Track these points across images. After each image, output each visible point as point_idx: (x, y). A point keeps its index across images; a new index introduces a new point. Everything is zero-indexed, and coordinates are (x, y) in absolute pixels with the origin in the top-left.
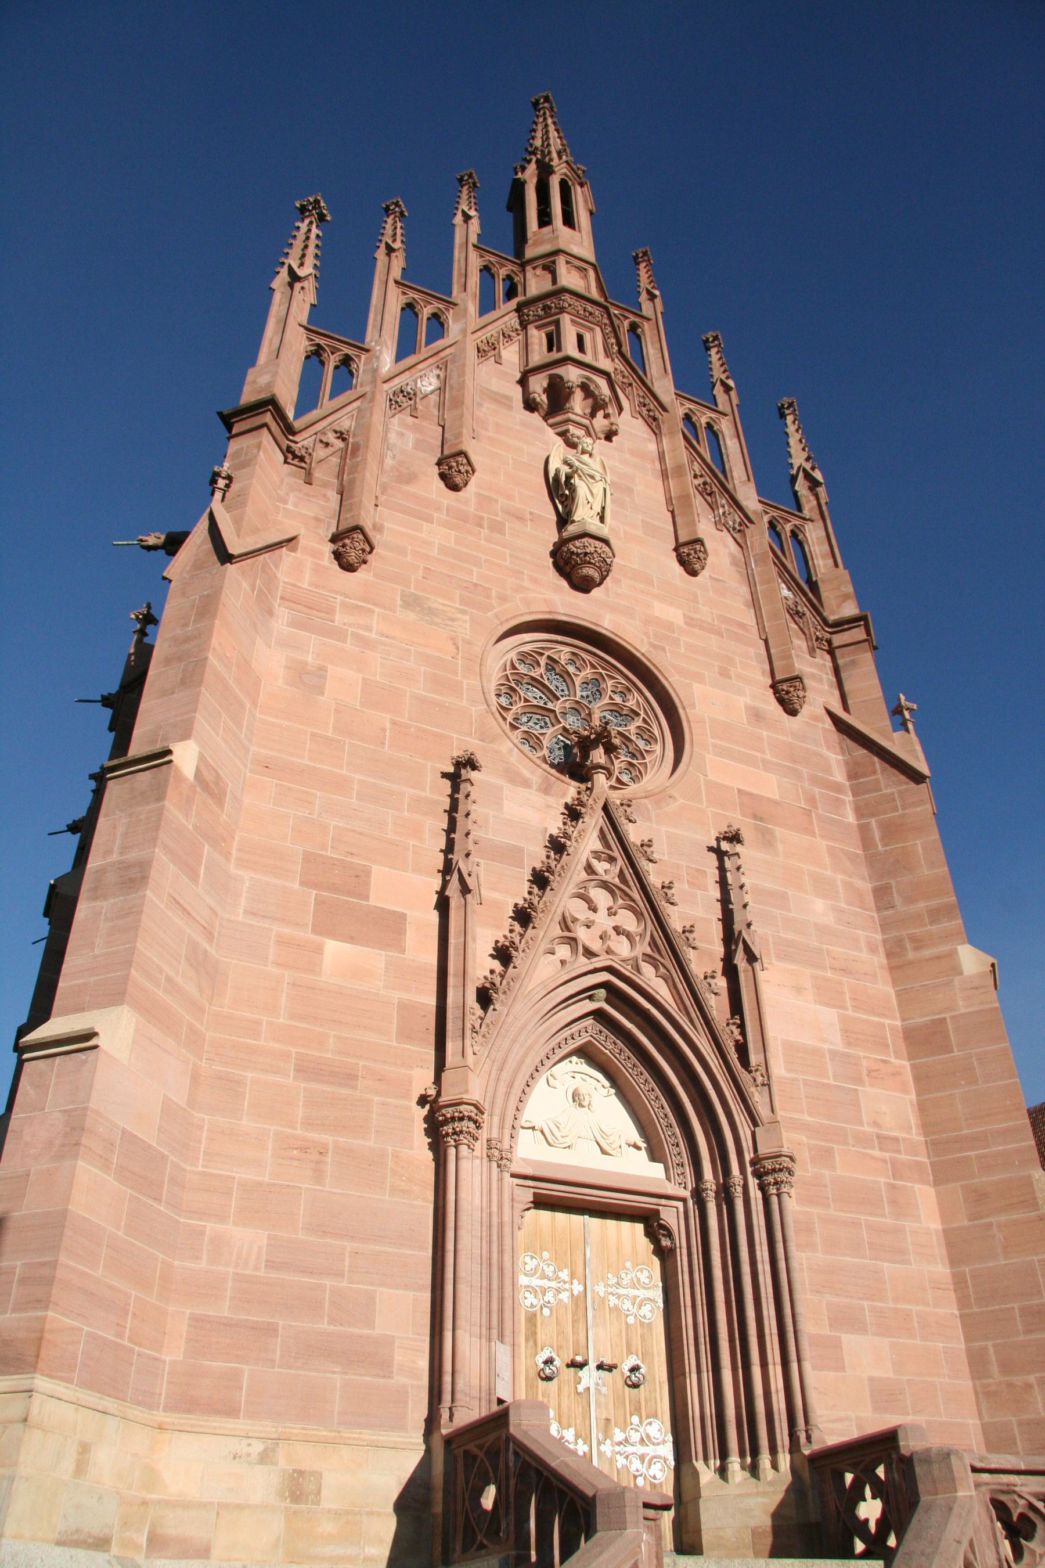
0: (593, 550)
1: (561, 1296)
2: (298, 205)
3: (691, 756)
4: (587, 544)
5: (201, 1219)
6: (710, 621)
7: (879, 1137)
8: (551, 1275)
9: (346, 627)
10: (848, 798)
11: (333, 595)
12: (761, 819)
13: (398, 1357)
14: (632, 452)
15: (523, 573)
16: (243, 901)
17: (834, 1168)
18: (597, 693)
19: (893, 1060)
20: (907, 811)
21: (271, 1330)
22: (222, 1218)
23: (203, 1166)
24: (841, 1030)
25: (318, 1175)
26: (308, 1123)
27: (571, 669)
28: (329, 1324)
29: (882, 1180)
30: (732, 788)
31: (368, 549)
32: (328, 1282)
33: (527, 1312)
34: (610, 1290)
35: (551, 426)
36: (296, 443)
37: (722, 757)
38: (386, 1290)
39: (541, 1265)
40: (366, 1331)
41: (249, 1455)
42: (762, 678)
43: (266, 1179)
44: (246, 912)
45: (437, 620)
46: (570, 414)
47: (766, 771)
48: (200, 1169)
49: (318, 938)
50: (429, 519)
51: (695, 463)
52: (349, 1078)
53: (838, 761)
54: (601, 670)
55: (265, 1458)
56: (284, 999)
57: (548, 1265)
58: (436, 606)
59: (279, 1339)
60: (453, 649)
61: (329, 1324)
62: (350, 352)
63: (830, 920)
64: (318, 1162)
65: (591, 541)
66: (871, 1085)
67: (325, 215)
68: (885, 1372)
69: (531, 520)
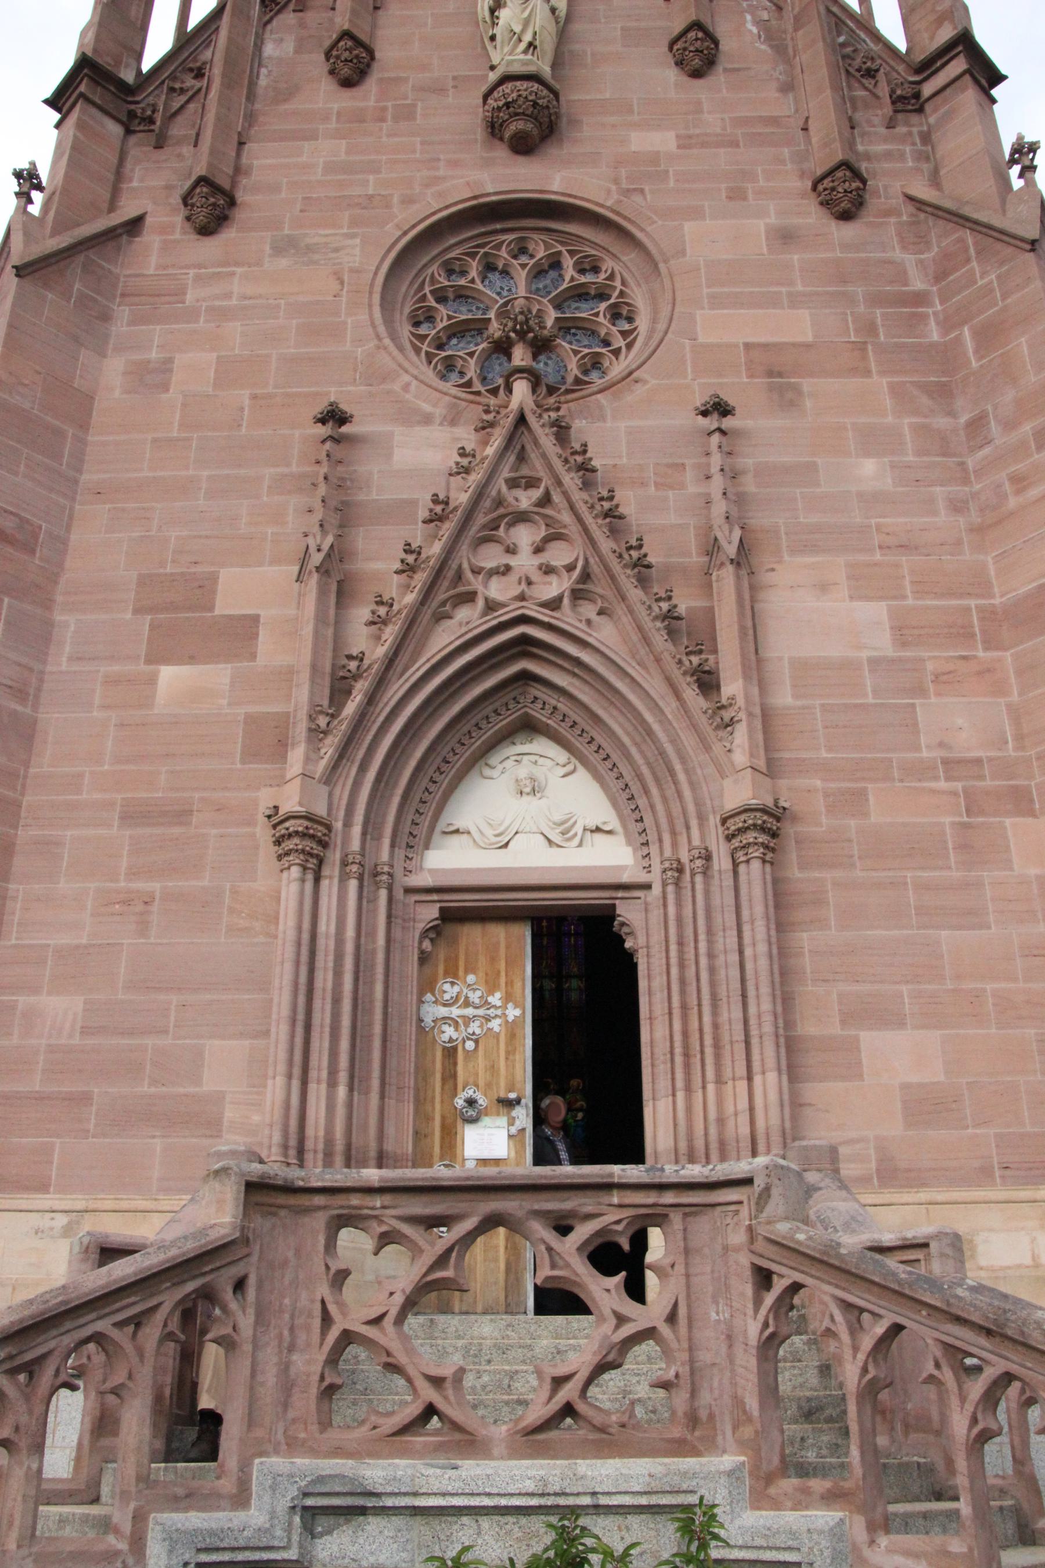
1: (490, 1025)
5: (13, 994)
6: (718, 130)
7: (946, 762)
8: (477, 1001)
11: (246, 302)
12: (780, 375)
13: (230, 1114)
15: (439, 160)
16: (67, 649)
17: (866, 815)
19: (981, 654)
20: (1009, 300)
21: (85, 1098)
22: (35, 990)
23: (17, 939)
24: (892, 628)
25: (143, 927)
26: (133, 873)
28: (150, 1085)
29: (948, 820)
30: (736, 346)
32: (149, 1041)
33: (444, 1048)
34: (499, 1012)
36: (137, 103)
38: (217, 1042)
39: (465, 991)
40: (192, 1090)
41: (52, 1229)
42: (799, 184)
43: (84, 941)
44: (70, 659)
45: (316, 257)
48: (14, 942)
49: (152, 667)
50: (313, 136)
52: (182, 815)
54: (482, 251)
55: (67, 1231)
56: (110, 743)
57: (474, 990)
58: (316, 240)
59: (94, 1108)
60: (335, 286)
61: (150, 1085)
63: (887, 483)
64: (142, 914)
66: (938, 694)
68: (935, 1073)
69: (455, 87)
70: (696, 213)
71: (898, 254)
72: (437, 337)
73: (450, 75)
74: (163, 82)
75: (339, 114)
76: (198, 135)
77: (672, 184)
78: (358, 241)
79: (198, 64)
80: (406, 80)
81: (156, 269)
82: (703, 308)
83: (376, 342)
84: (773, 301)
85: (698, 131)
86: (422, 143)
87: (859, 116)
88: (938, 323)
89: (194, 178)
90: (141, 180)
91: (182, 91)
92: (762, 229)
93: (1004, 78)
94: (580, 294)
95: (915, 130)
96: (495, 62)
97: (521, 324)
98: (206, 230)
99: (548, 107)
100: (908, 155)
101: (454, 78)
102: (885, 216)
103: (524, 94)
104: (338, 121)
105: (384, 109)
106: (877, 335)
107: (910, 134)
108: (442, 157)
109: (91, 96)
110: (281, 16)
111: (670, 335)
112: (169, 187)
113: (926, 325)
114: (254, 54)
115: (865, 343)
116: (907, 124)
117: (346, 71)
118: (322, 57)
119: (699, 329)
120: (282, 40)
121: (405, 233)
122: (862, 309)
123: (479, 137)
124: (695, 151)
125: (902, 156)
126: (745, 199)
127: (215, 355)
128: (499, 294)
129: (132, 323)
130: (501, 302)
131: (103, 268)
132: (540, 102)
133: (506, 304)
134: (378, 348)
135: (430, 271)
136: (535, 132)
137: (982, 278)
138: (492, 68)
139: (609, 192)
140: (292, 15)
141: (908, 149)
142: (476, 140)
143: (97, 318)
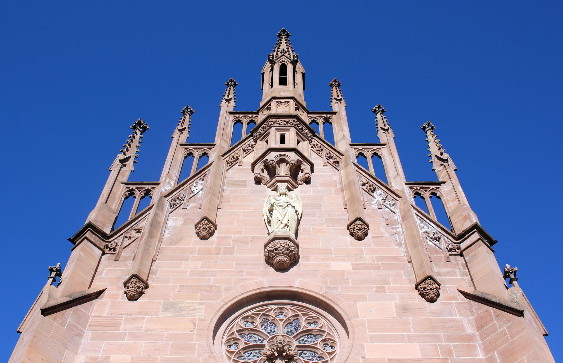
0: (279, 245)
2: (131, 127)
4: (275, 243)
6: (371, 262)
9: (126, 332)
10: (478, 343)
11: (121, 316)
14: (321, 185)
18: (272, 324)
20: (514, 339)
30: (384, 360)
35: (269, 188)
37: (377, 342)
42: (409, 285)
45: (184, 313)
46: (277, 178)
47: (411, 342)
51: (363, 177)
53: (469, 321)
54: (262, 313)
62: (147, 188)
67: (146, 127)
69: (251, 241)
72: (239, 353)
74: (122, 234)
75: (199, 250)
76: (134, 256)
77: (350, 285)
78: (204, 306)
79: (139, 228)
80: (230, 237)
81: (107, 314)
82: (368, 342)
83: (209, 354)
85: (362, 262)
86: (236, 264)
88: (481, 350)
89: (130, 275)
91: (130, 238)
92: (394, 305)
94: (307, 332)
96: (270, 232)
97: (280, 348)
98: (132, 299)
100: (458, 273)
101: (252, 237)
102: (450, 300)
103: (283, 245)
104: (198, 254)
105: (220, 249)
106: (453, 356)
108: (245, 270)
109: (90, 238)
111: (352, 355)
112: (118, 278)
114: (163, 225)
118: (194, 227)
119: (366, 352)
120: (176, 219)
121: (226, 303)
122: (444, 343)
126: (385, 292)
127: (130, 356)
128: (269, 333)
129: (94, 338)
130: (270, 337)
131: (82, 312)
132: (290, 248)
133: (272, 338)
134: (210, 357)
135: (237, 321)
136: (288, 261)
137: (500, 328)
138: (269, 234)
139: (321, 287)
140: (182, 210)
141: (457, 271)
142: (261, 264)
143: (76, 335)
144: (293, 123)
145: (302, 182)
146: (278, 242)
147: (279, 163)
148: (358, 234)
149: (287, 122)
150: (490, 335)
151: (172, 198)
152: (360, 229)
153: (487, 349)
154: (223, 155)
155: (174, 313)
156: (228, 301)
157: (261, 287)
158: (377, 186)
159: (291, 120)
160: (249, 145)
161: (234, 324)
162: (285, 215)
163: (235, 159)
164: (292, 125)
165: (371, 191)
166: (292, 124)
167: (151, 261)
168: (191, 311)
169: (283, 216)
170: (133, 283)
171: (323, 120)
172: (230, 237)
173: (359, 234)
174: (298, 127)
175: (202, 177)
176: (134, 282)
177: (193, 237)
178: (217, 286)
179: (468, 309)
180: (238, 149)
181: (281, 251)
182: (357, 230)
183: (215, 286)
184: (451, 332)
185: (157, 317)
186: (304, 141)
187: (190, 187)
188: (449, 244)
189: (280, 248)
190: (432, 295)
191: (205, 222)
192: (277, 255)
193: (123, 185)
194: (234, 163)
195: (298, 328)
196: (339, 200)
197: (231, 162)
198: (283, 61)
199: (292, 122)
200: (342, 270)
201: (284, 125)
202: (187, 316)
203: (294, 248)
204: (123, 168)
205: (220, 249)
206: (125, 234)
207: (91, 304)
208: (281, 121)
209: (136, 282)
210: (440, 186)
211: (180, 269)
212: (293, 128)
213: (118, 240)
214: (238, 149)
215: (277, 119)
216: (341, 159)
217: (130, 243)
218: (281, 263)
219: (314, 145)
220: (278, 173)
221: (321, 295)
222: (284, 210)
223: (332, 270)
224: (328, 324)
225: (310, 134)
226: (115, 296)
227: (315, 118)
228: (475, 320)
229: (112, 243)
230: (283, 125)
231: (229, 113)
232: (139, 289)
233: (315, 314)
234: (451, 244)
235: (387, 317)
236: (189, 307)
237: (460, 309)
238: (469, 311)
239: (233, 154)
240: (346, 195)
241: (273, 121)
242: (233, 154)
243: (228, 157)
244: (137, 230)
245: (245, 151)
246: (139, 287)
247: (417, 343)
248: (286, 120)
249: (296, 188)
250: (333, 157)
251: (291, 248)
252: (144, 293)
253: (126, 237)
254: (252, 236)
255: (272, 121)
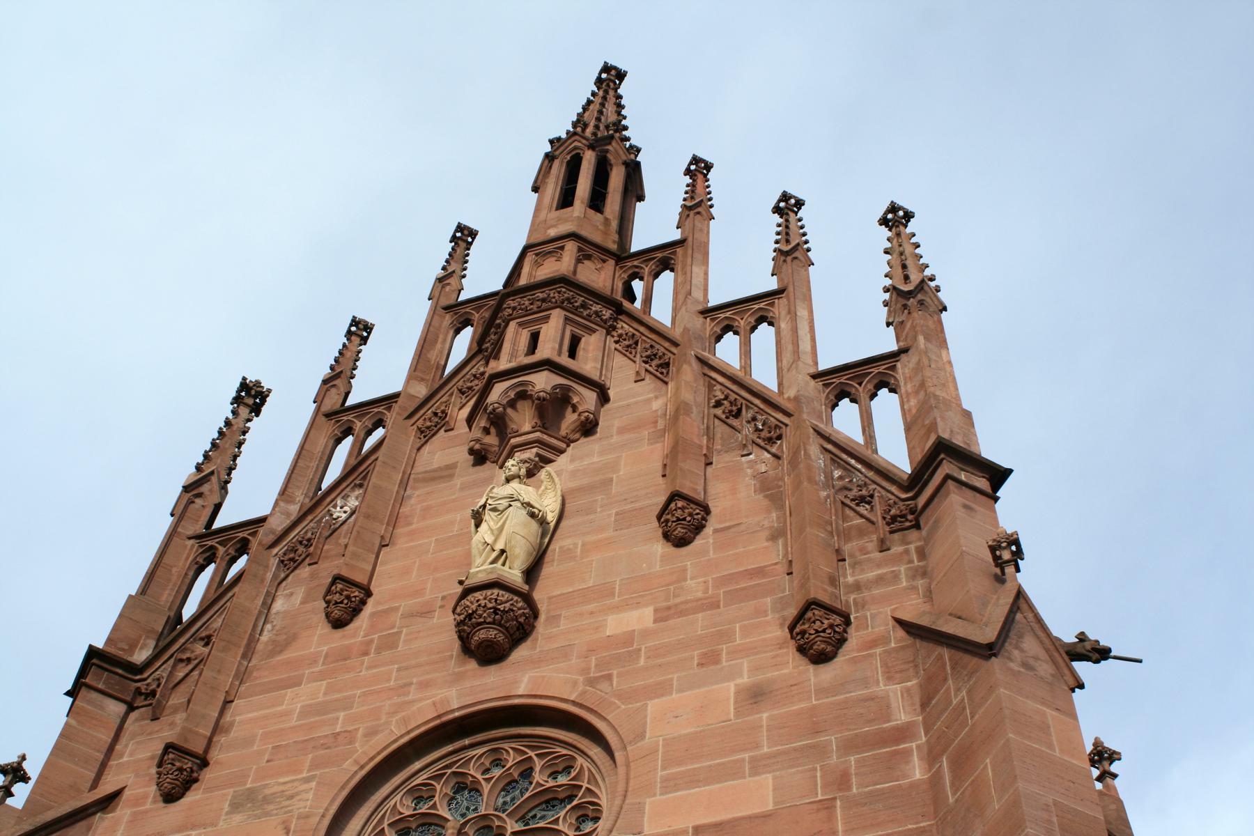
0: (474, 607)
3: (613, 727)
6: (700, 595)
14: (621, 431)
27: (424, 809)
30: (685, 831)
31: (837, 620)
45: (271, 807)
46: (513, 441)
65: (478, 595)
70: (662, 689)
71: (882, 687)
73: (440, 595)
84: (733, 772)
85: (678, 600)
87: (847, 548)
88: (921, 759)
90: (131, 755)
92: (732, 689)
93: (1009, 472)
95: (912, 547)
99: (512, 610)
102: (871, 648)
103: (483, 603)
107: (907, 552)
108: (415, 680)
110: (297, 572)
113: (907, 762)
114: (260, 613)
115: (835, 799)
116: (905, 542)
117: (337, 613)
119: (646, 819)
121: (362, 767)
122: (834, 759)
123: (455, 653)
124: (671, 622)
125: (896, 576)
132: (501, 607)
136: (501, 638)
144: (557, 298)
145: (577, 435)
146: (472, 599)
147: (512, 404)
148: (675, 533)
149: (543, 300)
150: (939, 718)
151: (286, 548)
152: (678, 519)
153: (932, 757)
154: (410, 416)
155: (251, 813)
156: (366, 759)
157: (442, 712)
158: (744, 402)
159: (552, 292)
160: (475, 376)
161: (386, 808)
162: (501, 529)
163: (440, 417)
164: (556, 302)
165: (733, 416)
166: (554, 300)
167: (220, 704)
168: (288, 799)
169: (496, 532)
170: (169, 764)
171: (653, 267)
172: (397, 609)
173: (677, 532)
174: (571, 303)
175: (358, 482)
176: (170, 761)
177: (319, 628)
178: (349, 732)
179: (909, 662)
180: (447, 392)
181: (480, 618)
182: (674, 524)
183: (346, 731)
184: (855, 729)
185: (215, 828)
186: (594, 331)
187: (329, 510)
188: (890, 506)
189: (477, 610)
190: (818, 645)
191: (336, 587)
192: (475, 628)
193: (192, 541)
194: (436, 429)
195: (474, 796)
196: (653, 454)
197: (428, 428)
198: (575, 148)
199: (554, 297)
200: (630, 629)
201: (538, 308)
202: (276, 815)
203: (512, 605)
204: (193, 502)
205: (372, 641)
206: (180, 654)
207: (89, 828)
208: (529, 300)
209: (173, 759)
210: (897, 361)
211: (279, 708)
212: (558, 309)
213: (162, 671)
214: (447, 392)
215: (521, 298)
216: (674, 354)
217: (187, 672)
218: (488, 645)
219: (620, 336)
220: (514, 427)
221: (574, 703)
222: (501, 518)
223: (608, 634)
224: (590, 766)
225: (607, 314)
226: (138, 801)
227: (637, 267)
228: (921, 686)
229: (149, 681)
230: (535, 309)
231: (443, 309)
232: (182, 774)
233: (566, 748)
234: (895, 503)
235: (712, 724)
236: (283, 791)
237: (890, 665)
238: (912, 665)
239: (433, 409)
240: (668, 440)
241: (512, 305)
242: (433, 409)
243: (423, 418)
244: (206, 640)
245: (463, 393)
246: (181, 770)
247: (770, 772)
248: (541, 296)
249: (562, 452)
250: (657, 353)
251: (503, 605)
252: (196, 780)
253: (181, 660)
254: (445, 593)
255: (509, 308)
